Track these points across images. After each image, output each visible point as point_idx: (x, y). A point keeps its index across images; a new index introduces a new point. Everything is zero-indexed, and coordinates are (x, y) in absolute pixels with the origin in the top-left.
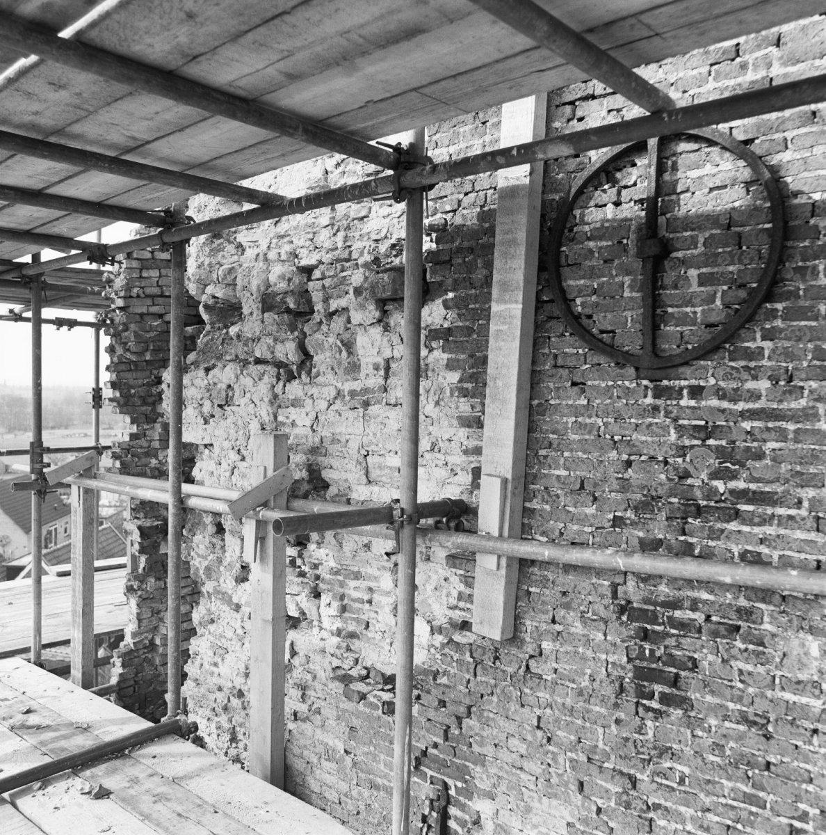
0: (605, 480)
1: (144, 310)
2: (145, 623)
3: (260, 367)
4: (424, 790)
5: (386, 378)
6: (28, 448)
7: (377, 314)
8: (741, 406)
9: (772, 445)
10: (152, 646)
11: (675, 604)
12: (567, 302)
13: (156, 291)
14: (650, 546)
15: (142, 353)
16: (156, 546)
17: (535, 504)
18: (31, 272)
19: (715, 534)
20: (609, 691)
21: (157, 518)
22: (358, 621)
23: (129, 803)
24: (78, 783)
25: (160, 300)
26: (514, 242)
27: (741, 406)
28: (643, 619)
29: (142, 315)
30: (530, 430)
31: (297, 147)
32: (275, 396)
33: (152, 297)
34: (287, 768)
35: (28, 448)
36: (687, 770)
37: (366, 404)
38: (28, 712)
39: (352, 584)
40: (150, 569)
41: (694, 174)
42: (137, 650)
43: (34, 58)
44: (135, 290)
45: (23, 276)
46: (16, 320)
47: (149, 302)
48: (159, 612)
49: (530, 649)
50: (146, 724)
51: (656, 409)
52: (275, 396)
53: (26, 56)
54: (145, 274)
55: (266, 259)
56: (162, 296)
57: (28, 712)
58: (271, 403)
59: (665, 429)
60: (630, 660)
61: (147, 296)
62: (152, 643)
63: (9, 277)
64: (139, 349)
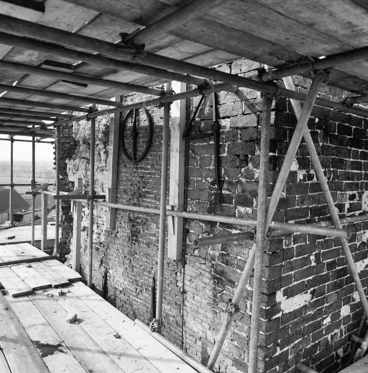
0: (128, 189)
1: (64, 141)
2: (64, 236)
3: (83, 160)
4: (103, 269)
5: (106, 163)
6: (31, 183)
7: (103, 146)
8: (147, 172)
9: (151, 180)
10: (66, 243)
11: (137, 218)
12: (124, 146)
13: (68, 135)
14: (135, 205)
15: (64, 154)
16: (68, 213)
17: (118, 195)
18: (31, 130)
19: (143, 201)
20: (127, 239)
21: (68, 204)
22: (100, 230)
23: (35, 268)
24: (26, 264)
25: (69, 138)
26: (112, 131)
27: (147, 172)
28: (132, 221)
29: (63, 143)
30: (118, 177)
31: (107, 88)
32: (86, 168)
33: (67, 137)
34: (81, 268)
35: (31, 183)
36: (138, 257)
37: (103, 170)
38: (23, 253)
39: (99, 219)
40: (66, 220)
41: (142, 117)
42: (61, 244)
43: (6, 92)
44: (61, 136)
45: (29, 132)
46: (38, 142)
47: (65, 139)
48: (69, 233)
49: (116, 231)
50: (46, 255)
51: (136, 172)
52: (86, 168)
53: (3, 92)
54: (64, 130)
55: (85, 129)
56: (70, 137)
57: (23, 253)
58: (85, 170)
59: (137, 177)
60: (131, 232)
61: (65, 137)
62: (66, 241)
63: (26, 132)
64: (63, 153)
